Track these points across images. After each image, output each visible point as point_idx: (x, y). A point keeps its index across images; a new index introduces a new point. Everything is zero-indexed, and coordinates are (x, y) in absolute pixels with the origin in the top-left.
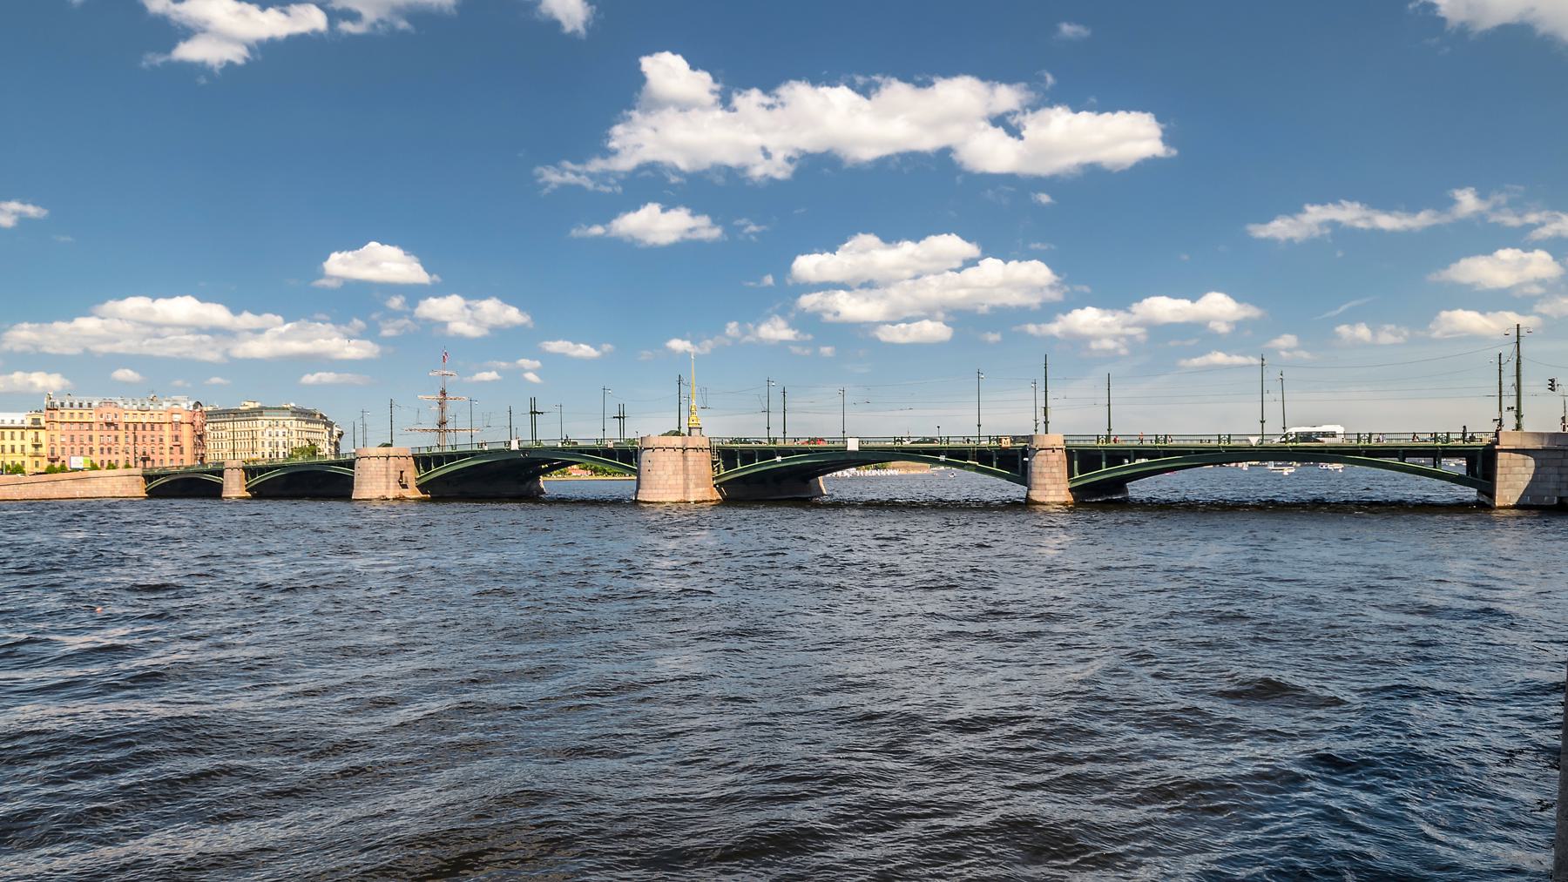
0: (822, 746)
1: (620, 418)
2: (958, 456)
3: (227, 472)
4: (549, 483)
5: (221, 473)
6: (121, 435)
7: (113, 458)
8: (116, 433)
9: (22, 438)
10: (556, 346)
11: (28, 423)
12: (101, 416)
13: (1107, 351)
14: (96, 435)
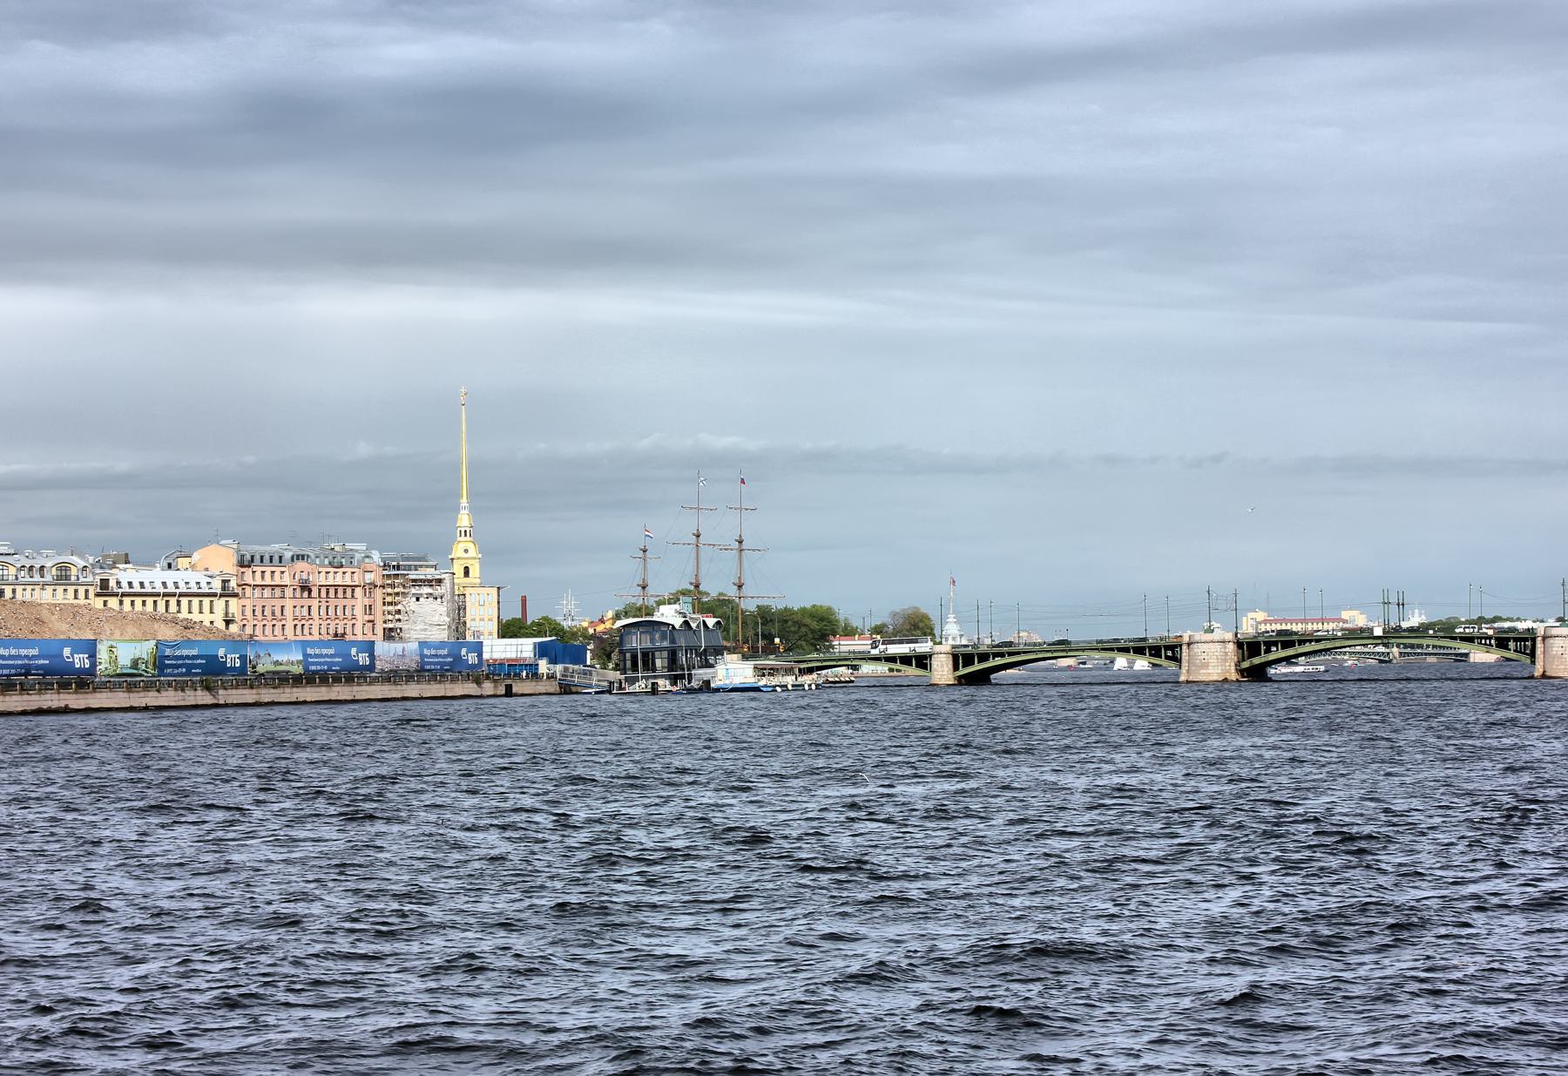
8: (308, 602)
14: (289, 604)
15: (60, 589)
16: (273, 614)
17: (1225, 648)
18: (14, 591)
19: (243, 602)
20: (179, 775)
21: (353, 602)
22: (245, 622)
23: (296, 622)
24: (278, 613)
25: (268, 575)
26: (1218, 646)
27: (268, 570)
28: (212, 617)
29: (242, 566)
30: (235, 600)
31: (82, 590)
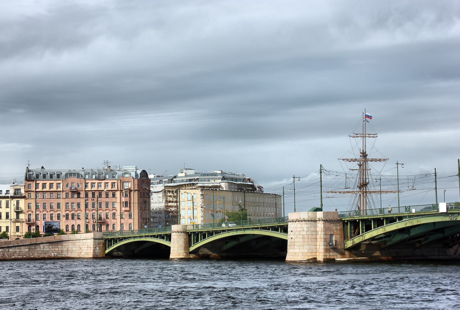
0: (323, 296)
2: (144, 173)
3: (291, 227)
6: (82, 202)
7: (76, 222)
8: (78, 200)
9: (7, 207)
11: (12, 193)
12: (67, 185)
14: (63, 202)
16: (51, 207)
17: (316, 227)
19: (29, 201)
21: (114, 200)
22: (30, 212)
23: (67, 212)
24: (55, 207)
26: (305, 225)
27: (48, 183)
28: (8, 210)
29: (28, 181)
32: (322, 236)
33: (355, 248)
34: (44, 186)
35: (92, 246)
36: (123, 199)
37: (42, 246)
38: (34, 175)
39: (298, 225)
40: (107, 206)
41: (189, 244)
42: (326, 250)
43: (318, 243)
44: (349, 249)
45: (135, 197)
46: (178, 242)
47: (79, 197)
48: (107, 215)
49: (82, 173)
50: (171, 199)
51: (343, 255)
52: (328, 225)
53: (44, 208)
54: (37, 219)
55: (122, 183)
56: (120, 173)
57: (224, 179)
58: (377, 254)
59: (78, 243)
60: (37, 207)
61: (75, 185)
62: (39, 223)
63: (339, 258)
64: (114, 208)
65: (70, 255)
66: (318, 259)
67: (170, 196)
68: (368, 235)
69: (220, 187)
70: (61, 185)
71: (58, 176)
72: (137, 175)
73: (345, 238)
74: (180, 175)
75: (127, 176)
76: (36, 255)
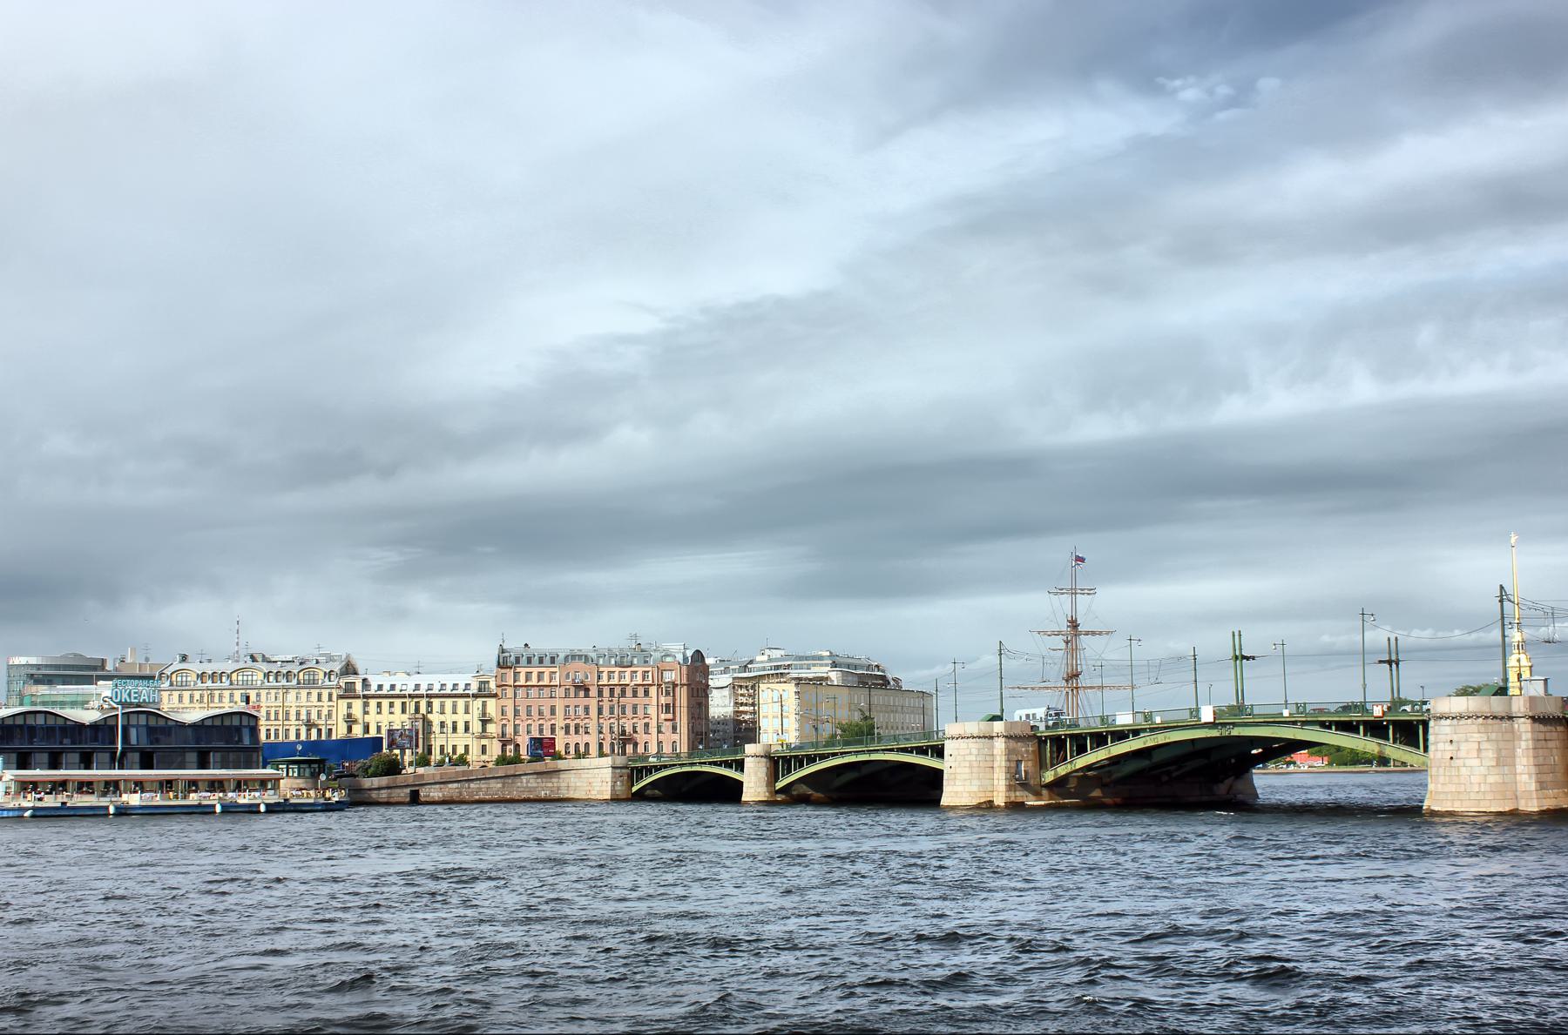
1: (1390, 662)
4: (1268, 782)
5: (939, 752)
6: (593, 704)
7: (582, 739)
10: (1391, 727)
12: (568, 676)
13: (779, 795)
15: (304, 693)
16: (540, 713)
17: (992, 747)
18: (258, 695)
19: (503, 702)
20: (1386, 880)
21: (646, 700)
22: (504, 722)
23: (568, 721)
25: (534, 676)
26: (973, 745)
27: (535, 671)
28: (468, 717)
29: (502, 668)
30: (493, 700)
31: (325, 694)
32: (1003, 764)
33: (1059, 784)
34: (528, 676)
35: (609, 780)
36: (663, 700)
37: (524, 779)
38: (513, 659)
39: (962, 743)
40: (635, 712)
41: (774, 776)
42: (1010, 788)
43: (996, 776)
44: (1050, 786)
45: (682, 695)
46: (756, 774)
47: (587, 696)
48: (634, 728)
49: (594, 655)
50: (744, 700)
51: (1038, 795)
52: (1012, 744)
53: (529, 714)
54: (516, 732)
55: (661, 672)
56: (657, 655)
57: (834, 665)
58: (1097, 793)
59: (585, 775)
60: (516, 713)
61: (580, 676)
62: (519, 740)
63: (1032, 802)
64: (646, 716)
65: (571, 795)
66: (996, 803)
67: (742, 695)
68: (1082, 762)
69: (827, 678)
70: (558, 674)
71: (553, 660)
72: (685, 659)
73: (1042, 766)
74: (759, 658)
75: (669, 659)
76: (515, 795)
